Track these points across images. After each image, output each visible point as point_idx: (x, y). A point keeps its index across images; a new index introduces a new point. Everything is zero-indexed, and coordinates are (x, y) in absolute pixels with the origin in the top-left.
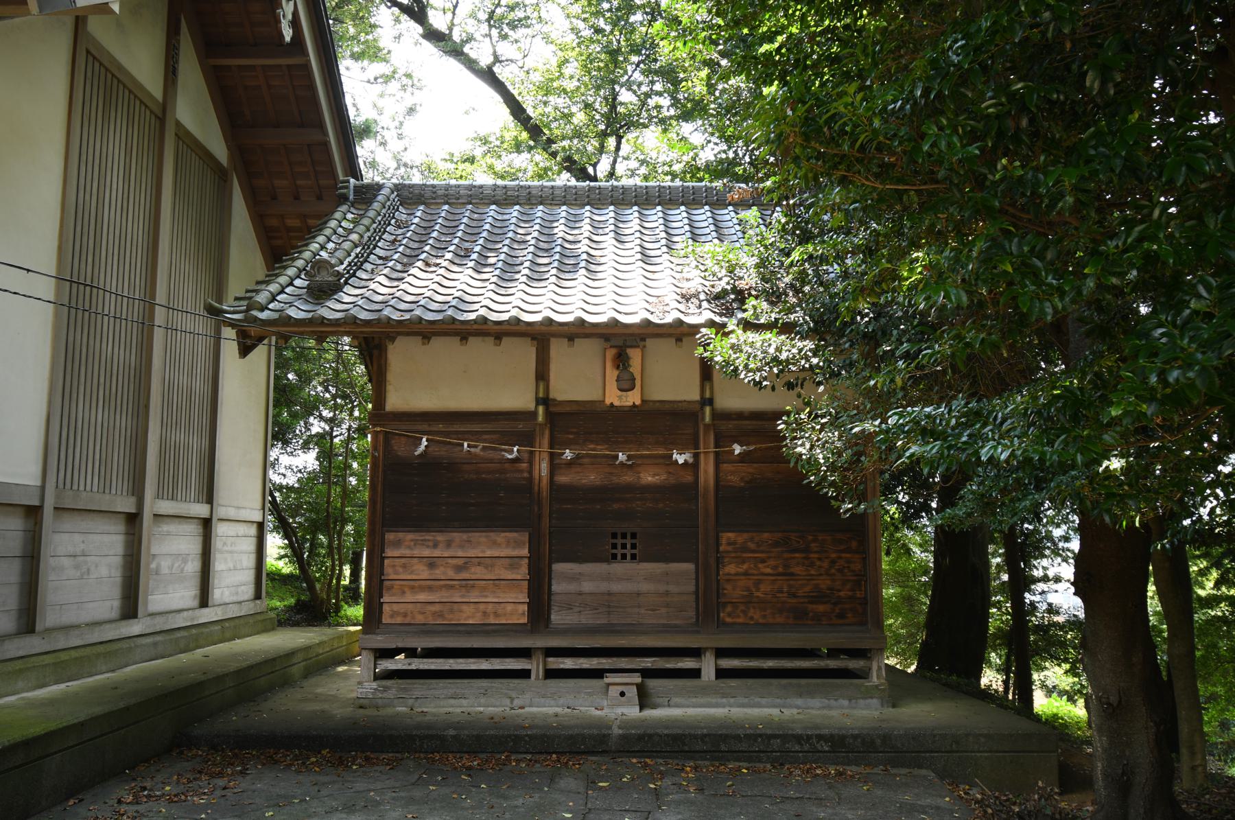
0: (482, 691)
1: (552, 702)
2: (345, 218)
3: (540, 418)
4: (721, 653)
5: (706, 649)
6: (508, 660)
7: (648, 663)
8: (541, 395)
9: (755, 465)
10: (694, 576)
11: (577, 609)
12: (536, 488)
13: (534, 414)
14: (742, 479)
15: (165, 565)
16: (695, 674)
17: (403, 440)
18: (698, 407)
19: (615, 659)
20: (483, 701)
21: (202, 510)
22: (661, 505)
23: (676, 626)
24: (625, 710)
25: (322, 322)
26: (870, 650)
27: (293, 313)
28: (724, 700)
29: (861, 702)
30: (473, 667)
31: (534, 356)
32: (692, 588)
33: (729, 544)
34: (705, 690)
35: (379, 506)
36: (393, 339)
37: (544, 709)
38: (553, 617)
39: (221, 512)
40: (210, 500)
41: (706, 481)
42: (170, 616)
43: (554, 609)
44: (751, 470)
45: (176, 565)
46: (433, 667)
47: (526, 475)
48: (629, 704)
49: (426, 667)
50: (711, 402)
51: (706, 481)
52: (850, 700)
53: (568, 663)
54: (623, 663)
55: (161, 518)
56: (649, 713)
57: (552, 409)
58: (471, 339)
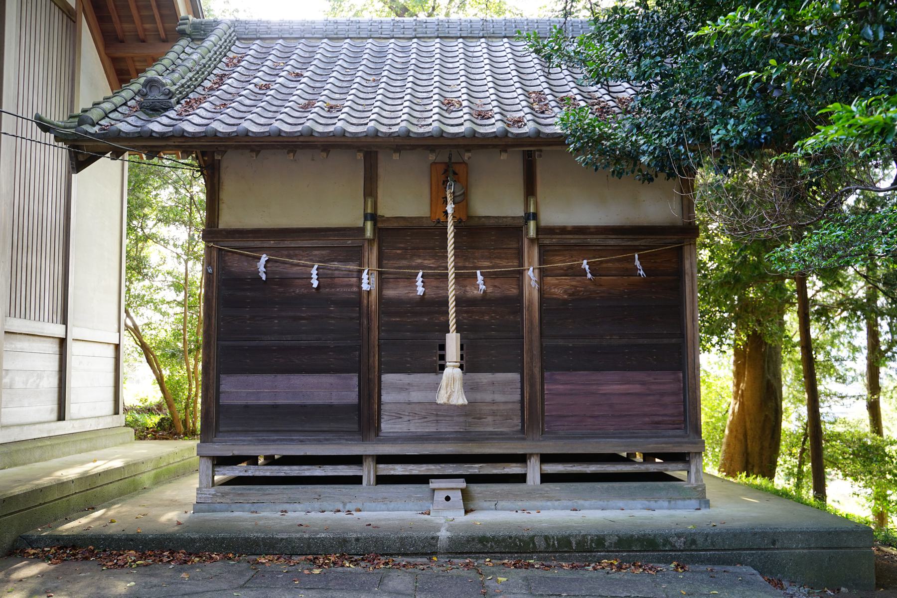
0: (317, 497)
1: (384, 507)
2: (183, 52)
3: (369, 233)
4: (545, 459)
5: (531, 455)
6: (340, 467)
7: (475, 469)
8: (369, 211)
9: (578, 278)
10: (519, 385)
11: (407, 418)
12: (365, 302)
13: (362, 230)
14: (565, 292)
15: (19, 381)
16: (521, 478)
17: (236, 257)
18: (522, 222)
19: (443, 465)
20: (317, 504)
21: (58, 330)
22: (487, 318)
23: (502, 433)
24: (450, 515)
25: (151, 136)
26: (689, 453)
27: (124, 127)
28: (549, 503)
29: (680, 503)
30: (307, 473)
31: (362, 174)
32: (517, 397)
33: (790, 102)
34: (530, 495)
35: (214, 321)
36: (223, 153)
37: (375, 513)
38: (383, 425)
39: (74, 332)
40: (65, 321)
41: (530, 294)
42: (25, 428)
43: (384, 418)
44: (574, 283)
45: (31, 380)
46: (268, 474)
47: (355, 289)
48: (453, 508)
49: (262, 474)
50: (535, 216)
51: (530, 294)
52: (669, 502)
53: (399, 470)
54: (450, 469)
55: (12, 336)
56: (471, 517)
57: (380, 225)
58: (299, 151)
